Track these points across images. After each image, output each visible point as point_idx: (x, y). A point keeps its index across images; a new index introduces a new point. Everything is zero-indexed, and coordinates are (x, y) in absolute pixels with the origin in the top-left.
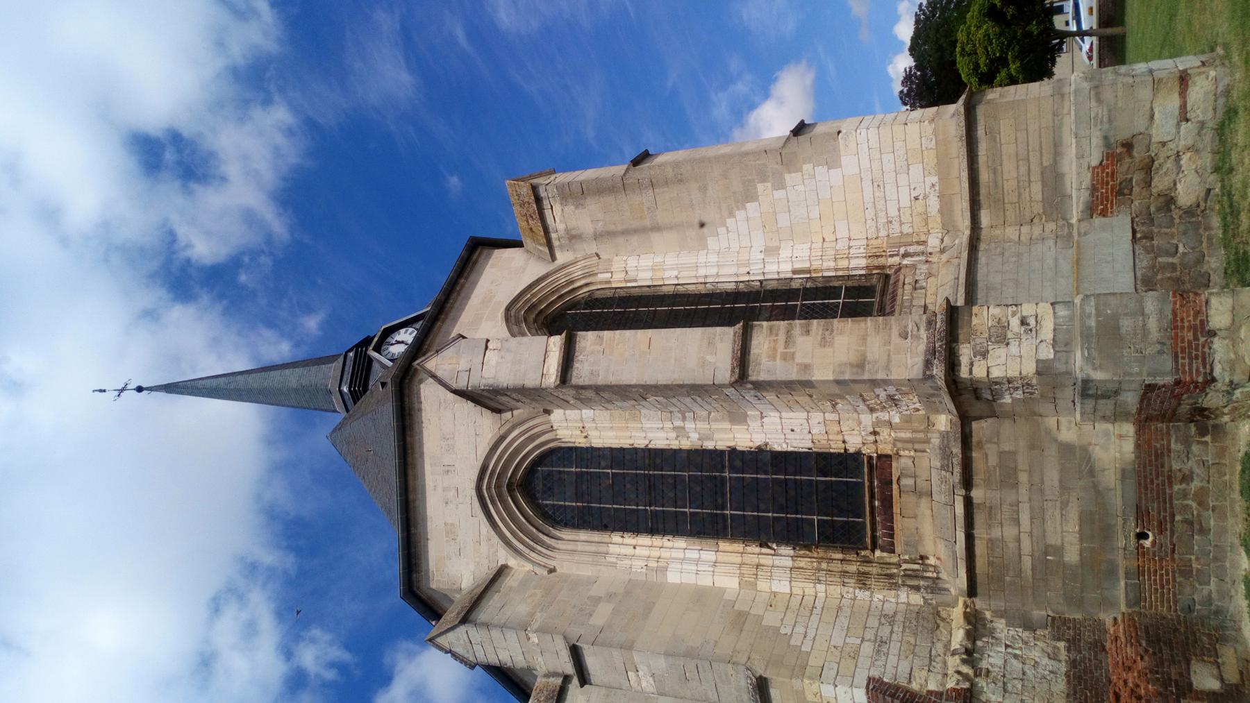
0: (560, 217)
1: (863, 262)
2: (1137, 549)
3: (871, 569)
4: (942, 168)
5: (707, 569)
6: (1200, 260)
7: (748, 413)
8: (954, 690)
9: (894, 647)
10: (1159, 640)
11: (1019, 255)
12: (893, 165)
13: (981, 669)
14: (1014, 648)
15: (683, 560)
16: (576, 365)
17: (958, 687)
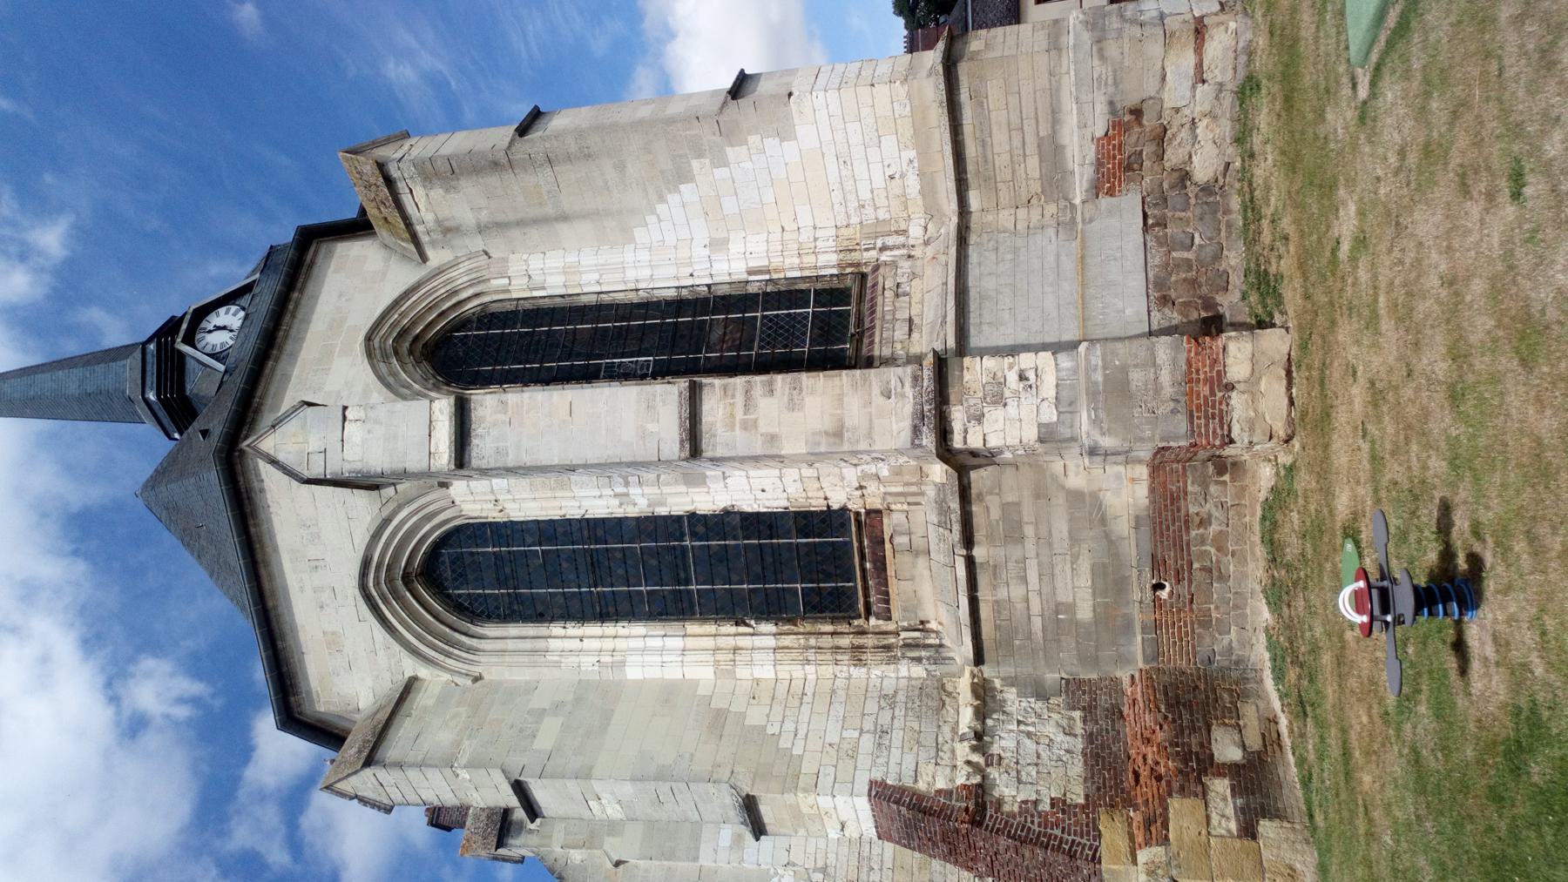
0: (424, 204)
1: (833, 258)
2: (1154, 601)
3: (866, 641)
4: (920, 139)
6: (1218, 256)
7: (708, 473)
8: (965, 786)
9: (897, 736)
10: (1178, 703)
11: (1015, 250)
12: (861, 137)
13: (992, 755)
14: (1026, 724)
15: (644, 650)
16: (475, 441)
17: (968, 783)
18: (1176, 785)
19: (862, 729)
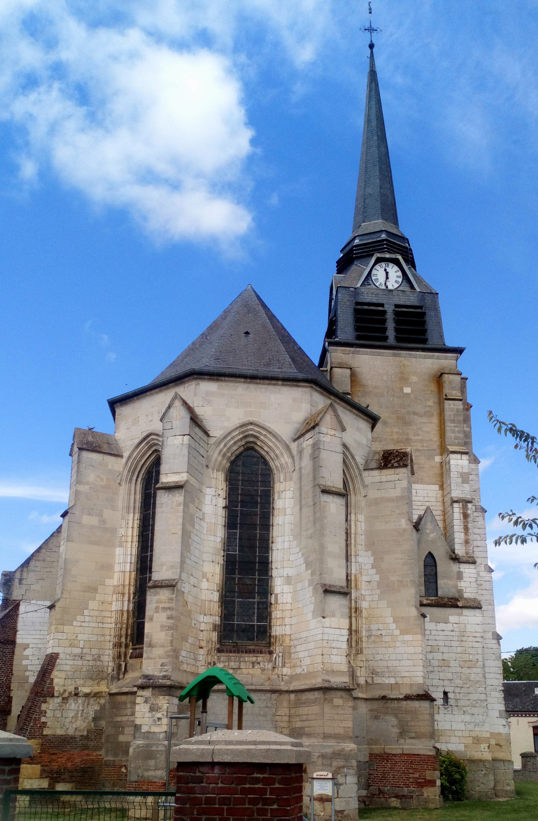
5: (121, 568)
9: (80, 663)
11: (265, 715)
17: (55, 691)
18: (46, 768)
19: (84, 648)
